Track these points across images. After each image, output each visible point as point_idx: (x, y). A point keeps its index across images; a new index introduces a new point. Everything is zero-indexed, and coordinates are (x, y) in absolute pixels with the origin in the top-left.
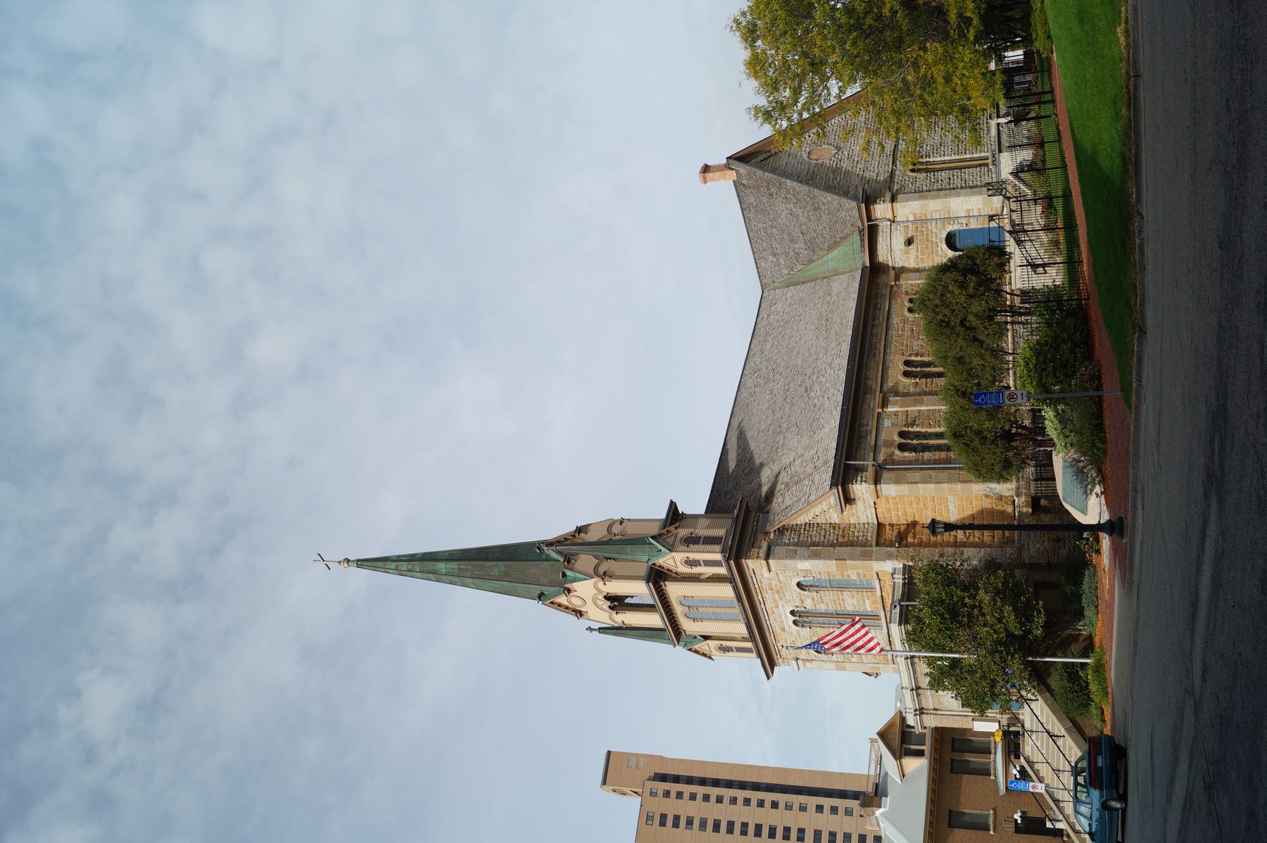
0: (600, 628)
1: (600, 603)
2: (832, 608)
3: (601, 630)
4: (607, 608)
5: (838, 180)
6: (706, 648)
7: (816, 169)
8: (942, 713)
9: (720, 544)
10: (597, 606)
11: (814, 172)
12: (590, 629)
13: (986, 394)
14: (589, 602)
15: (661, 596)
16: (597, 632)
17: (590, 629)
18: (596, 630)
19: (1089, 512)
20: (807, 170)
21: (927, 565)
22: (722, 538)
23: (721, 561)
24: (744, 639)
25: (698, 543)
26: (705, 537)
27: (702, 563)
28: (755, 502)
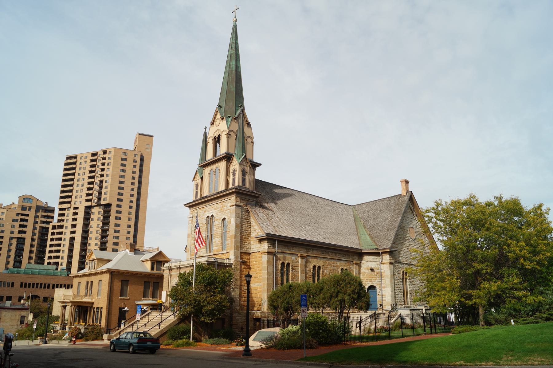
1: (217, 132)
2: (214, 232)
3: (205, 133)
8: (170, 278)
10: (216, 131)
12: (206, 128)
14: (217, 128)
16: (204, 131)
17: (206, 128)
18: (205, 131)
22: (245, 186)
25: (243, 176)
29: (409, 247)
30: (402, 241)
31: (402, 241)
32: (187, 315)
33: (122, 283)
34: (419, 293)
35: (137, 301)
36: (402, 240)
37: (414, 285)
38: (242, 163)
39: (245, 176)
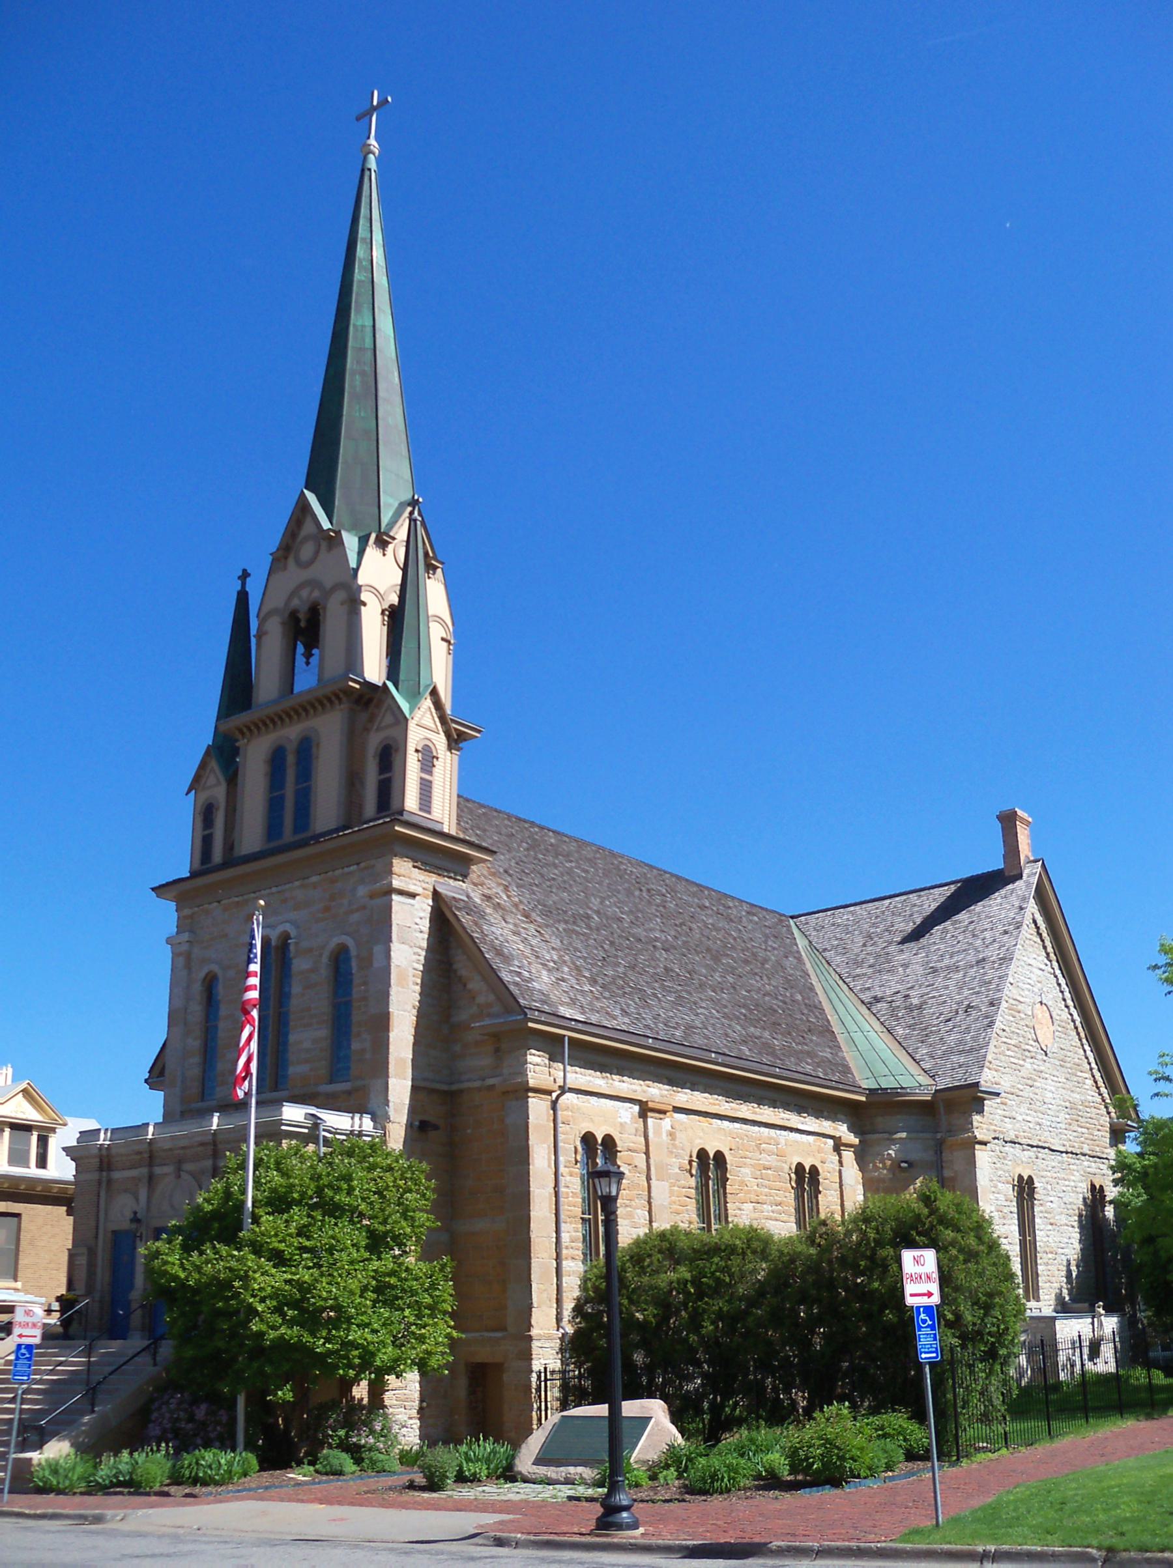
0: (247, 594)
1: (305, 593)
2: (295, 1003)
3: (243, 598)
4: (295, 602)
5: (1009, 1053)
6: (212, 780)
7: (1023, 1016)
8: (103, 1194)
9: (421, 809)
10: (301, 586)
11: (1019, 1012)
12: (245, 575)
13: (29, 1359)
14: (306, 574)
15: (281, 718)
16: (239, 588)
17: (245, 575)
18: (244, 585)
19: (535, 1467)
20: (1022, 999)
21: (267, 1198)
22: (429, 813)
23: (210, 862)
24: (229, 846)
25: (423, 770)
26: (431, 782)
27: (207, 832)
28: (479, 876)
29: (1035, 1081)
30: (1012, 1060)
31: (1012, 1060)
32: (267, 1340)
33: (184, 925)
34: (985, 1315)
35: (235, 1069)
36: (1012, 1054)
37: (1052, 1224)
38: (420, 719)
39: (430, 773)
